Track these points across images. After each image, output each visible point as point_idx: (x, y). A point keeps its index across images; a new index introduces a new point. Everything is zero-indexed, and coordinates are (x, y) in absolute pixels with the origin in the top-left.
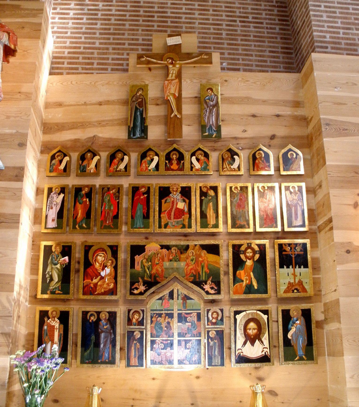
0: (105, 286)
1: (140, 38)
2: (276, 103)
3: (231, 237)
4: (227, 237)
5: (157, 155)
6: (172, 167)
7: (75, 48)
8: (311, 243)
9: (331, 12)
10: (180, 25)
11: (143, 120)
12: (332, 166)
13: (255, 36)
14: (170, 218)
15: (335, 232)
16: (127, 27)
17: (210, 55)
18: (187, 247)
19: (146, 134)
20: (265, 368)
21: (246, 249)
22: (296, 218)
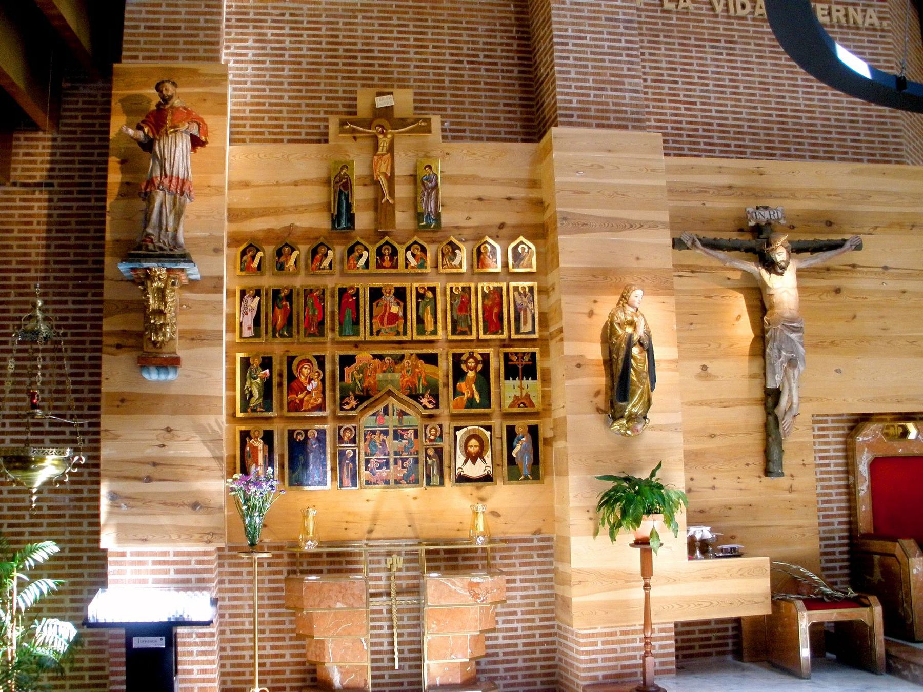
0: (312, 401)
1: (340, 89)
3: (452, 344)
4: (447, 345)
5: (366, 249)
6: (384, 264)
7: (258, 104)
8: (541, 352)
9: (581, 66)
10: (391, 69)
11: (349, 206)
12: (567, 269)
13: (486, 83)
14: (382, 324)
15: (565, 343)
16: (323, 73)
18: (402, 357)
19: (353, 224)
20: (487, 489)
21: (468, 359)
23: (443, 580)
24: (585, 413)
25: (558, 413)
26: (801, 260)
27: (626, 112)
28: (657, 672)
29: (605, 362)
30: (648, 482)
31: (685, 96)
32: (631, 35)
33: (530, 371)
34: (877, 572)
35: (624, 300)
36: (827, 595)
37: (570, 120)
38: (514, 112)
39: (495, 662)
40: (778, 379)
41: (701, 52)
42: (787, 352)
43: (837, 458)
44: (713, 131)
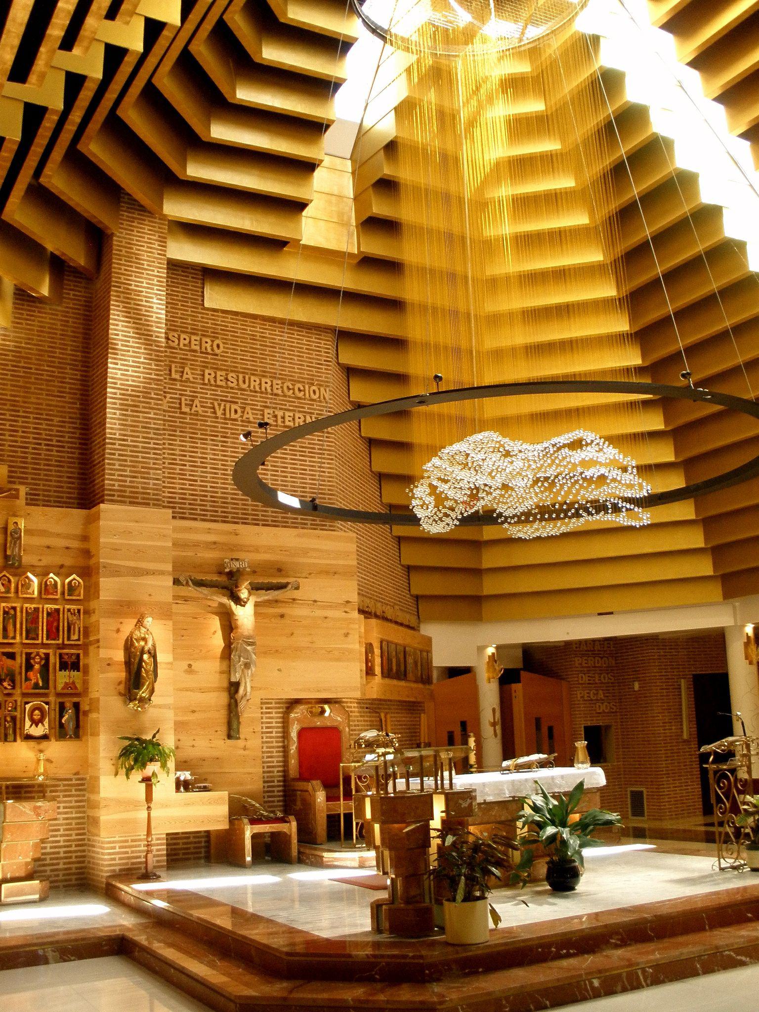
2: (67, 537)
12: (106, 601)
13: (56, 461)
17: (17, 490)
20: (44, 744)
21: (36, 656)
22: (74, 634)
23: (17, 805)
24: (112, 696)
25: (93, 695)
26: (258, 596)
27: (149, 494)
28: (155, 867)
29: (126, 663)
30: (151, 742)
31: (190, 475)
32: (157, 439)
33: (75, 666)
34: (299, 803)
35: (140, 623)
36: (264, 816)
37: (112, 498)
38: (73, 483)
39: (44, 865)
40: (238, 675)
41: (204, 444)
42: (244, 658)
43: (278, 727)
44: (207, 501)
